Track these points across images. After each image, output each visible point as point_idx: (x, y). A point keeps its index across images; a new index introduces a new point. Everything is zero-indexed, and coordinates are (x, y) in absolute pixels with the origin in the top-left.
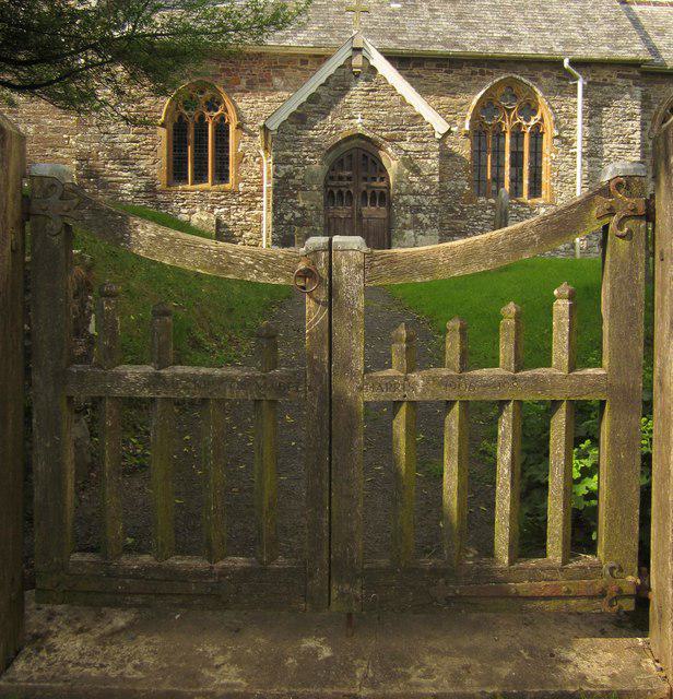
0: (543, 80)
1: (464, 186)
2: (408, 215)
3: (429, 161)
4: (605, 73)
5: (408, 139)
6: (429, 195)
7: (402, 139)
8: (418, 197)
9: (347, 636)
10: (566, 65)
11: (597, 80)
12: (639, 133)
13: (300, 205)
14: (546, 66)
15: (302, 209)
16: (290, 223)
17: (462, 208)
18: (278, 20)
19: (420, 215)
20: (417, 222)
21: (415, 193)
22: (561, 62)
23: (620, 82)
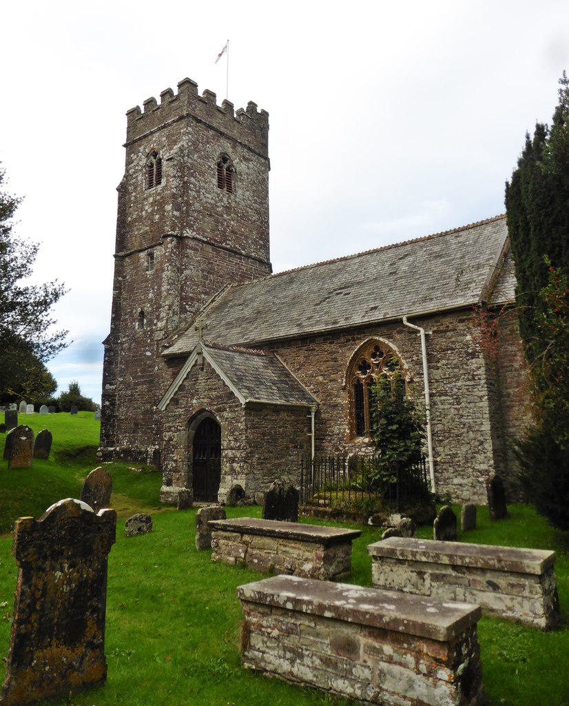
0: (398, 336)
1: (345, 429)
2: (228, 465)
3: (239, 425)
4: (447, 321)
5: (228, 409)
6: (239, 449)
7: (225, 410)
8: (234, 451)
9: (12, 672)
10: (405, 323)
11: (441, 328)
12: (483, 369)
13: (175, 458)
14: (391, 325)
15: (176, 461)
16: (170, 470)
17: (344, 447)
18: (528, 137)
19: (235, 465)
20: (232, 469)
21: (232, 449)
22: (401, 320)
23: (461, 326)
